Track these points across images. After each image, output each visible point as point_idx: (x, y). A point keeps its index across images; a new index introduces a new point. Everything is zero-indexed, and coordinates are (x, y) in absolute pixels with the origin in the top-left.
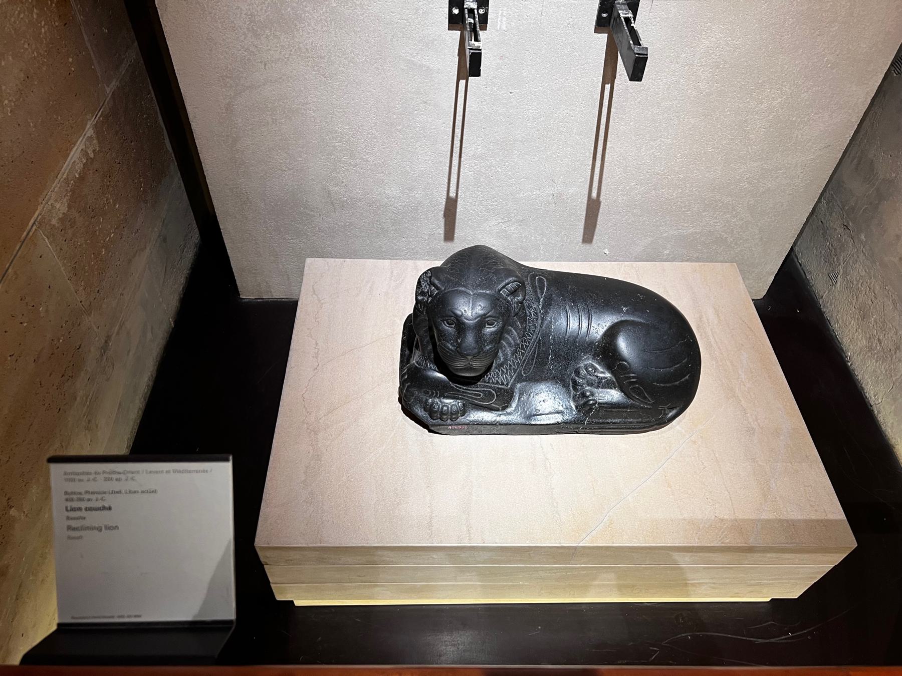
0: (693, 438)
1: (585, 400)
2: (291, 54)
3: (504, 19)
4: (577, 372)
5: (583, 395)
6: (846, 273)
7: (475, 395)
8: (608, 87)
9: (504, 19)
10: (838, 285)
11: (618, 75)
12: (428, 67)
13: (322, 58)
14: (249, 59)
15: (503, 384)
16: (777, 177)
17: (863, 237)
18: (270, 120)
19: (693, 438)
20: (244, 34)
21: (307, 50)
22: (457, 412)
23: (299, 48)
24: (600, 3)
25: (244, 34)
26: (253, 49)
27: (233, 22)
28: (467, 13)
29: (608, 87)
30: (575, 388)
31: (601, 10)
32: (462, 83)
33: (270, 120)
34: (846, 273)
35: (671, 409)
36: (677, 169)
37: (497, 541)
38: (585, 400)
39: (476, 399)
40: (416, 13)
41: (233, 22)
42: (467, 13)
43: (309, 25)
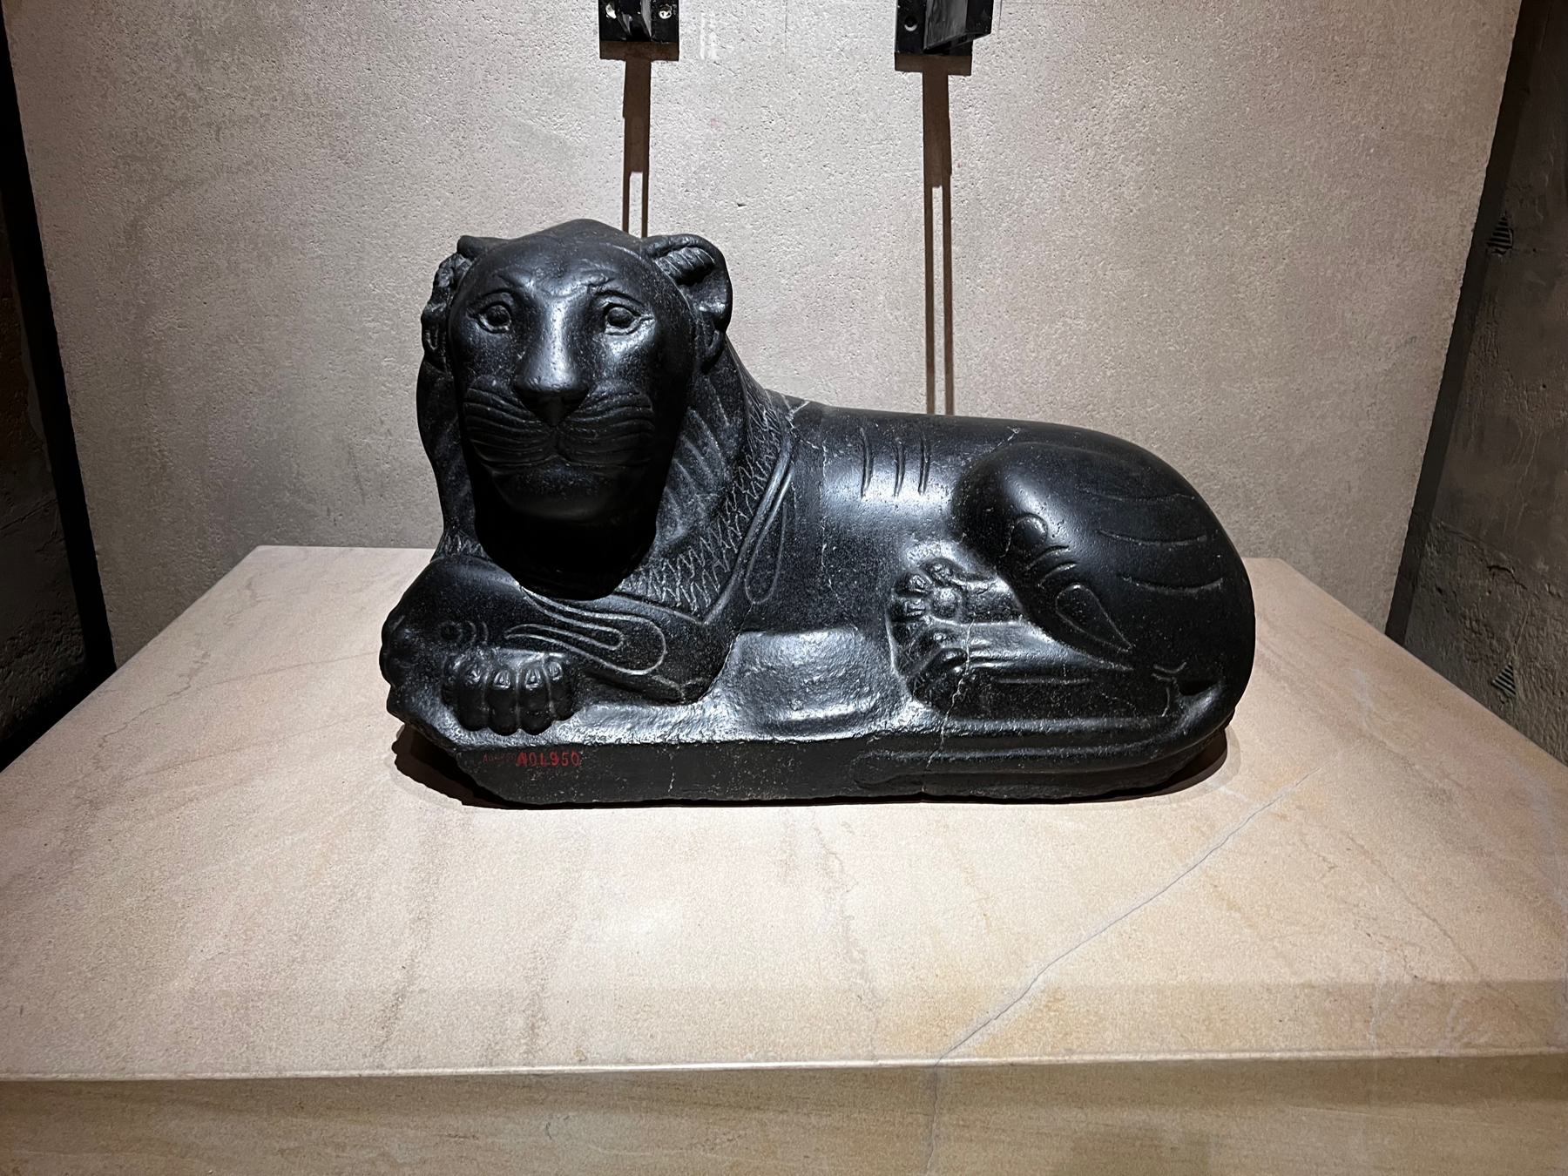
0: (1276, 808)
1: (931, 655)
2: (273, 108)
3: (713, 36)
4: (903, 587)
5: (927, 642)
6: (1528, 659)
7: (600, 636)
8: (938, 192)
9: (713, 36)
10: (1520, 692)
11: (954, 166)
12: (563, 142)
13: (340, 116)
14: (184, 119)
15: (685, 609)
16: (1323, 417)
17: (1540, 565)
18: (223, 264)
19: (1276, 808)
20: (178, 60)
21: (308, 98)
22: (542, 692)
23: (291, 93)
24: (899, 3)
25: (178, 60)
26: (192, 94)
27: (155, 32)
28: (638, 23)
29: (938, 192)
30: (901, 636)
31: (904, 16)
32: (637, 177)
33: (223, 264)
34: (1528, 659)
35: (1194, 689)
36: (1109, 395)
37: (635, 1053)
38: (931, 655)
39: (604, 654)
40: (532, 21)
41: (155, 32)
42: (638, 23)
43: (314, 41)
